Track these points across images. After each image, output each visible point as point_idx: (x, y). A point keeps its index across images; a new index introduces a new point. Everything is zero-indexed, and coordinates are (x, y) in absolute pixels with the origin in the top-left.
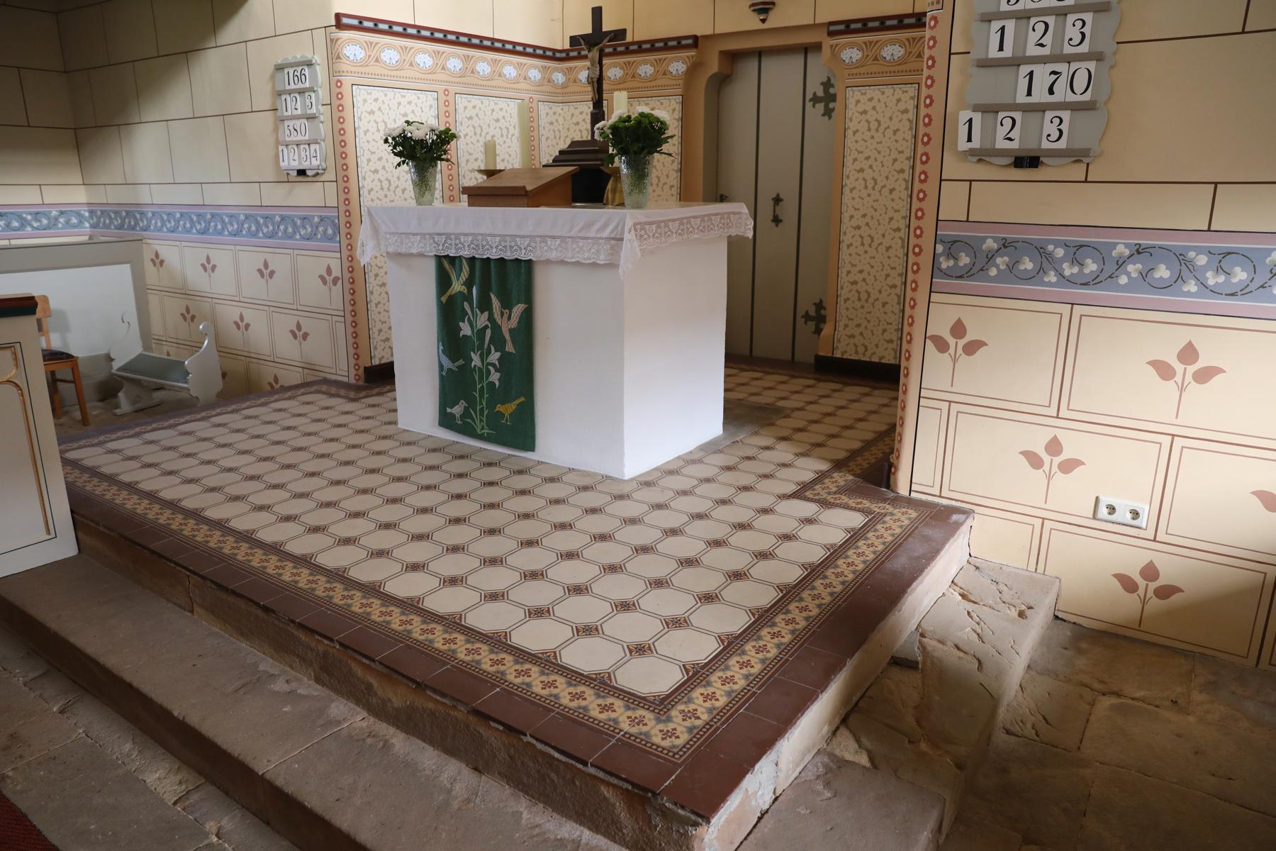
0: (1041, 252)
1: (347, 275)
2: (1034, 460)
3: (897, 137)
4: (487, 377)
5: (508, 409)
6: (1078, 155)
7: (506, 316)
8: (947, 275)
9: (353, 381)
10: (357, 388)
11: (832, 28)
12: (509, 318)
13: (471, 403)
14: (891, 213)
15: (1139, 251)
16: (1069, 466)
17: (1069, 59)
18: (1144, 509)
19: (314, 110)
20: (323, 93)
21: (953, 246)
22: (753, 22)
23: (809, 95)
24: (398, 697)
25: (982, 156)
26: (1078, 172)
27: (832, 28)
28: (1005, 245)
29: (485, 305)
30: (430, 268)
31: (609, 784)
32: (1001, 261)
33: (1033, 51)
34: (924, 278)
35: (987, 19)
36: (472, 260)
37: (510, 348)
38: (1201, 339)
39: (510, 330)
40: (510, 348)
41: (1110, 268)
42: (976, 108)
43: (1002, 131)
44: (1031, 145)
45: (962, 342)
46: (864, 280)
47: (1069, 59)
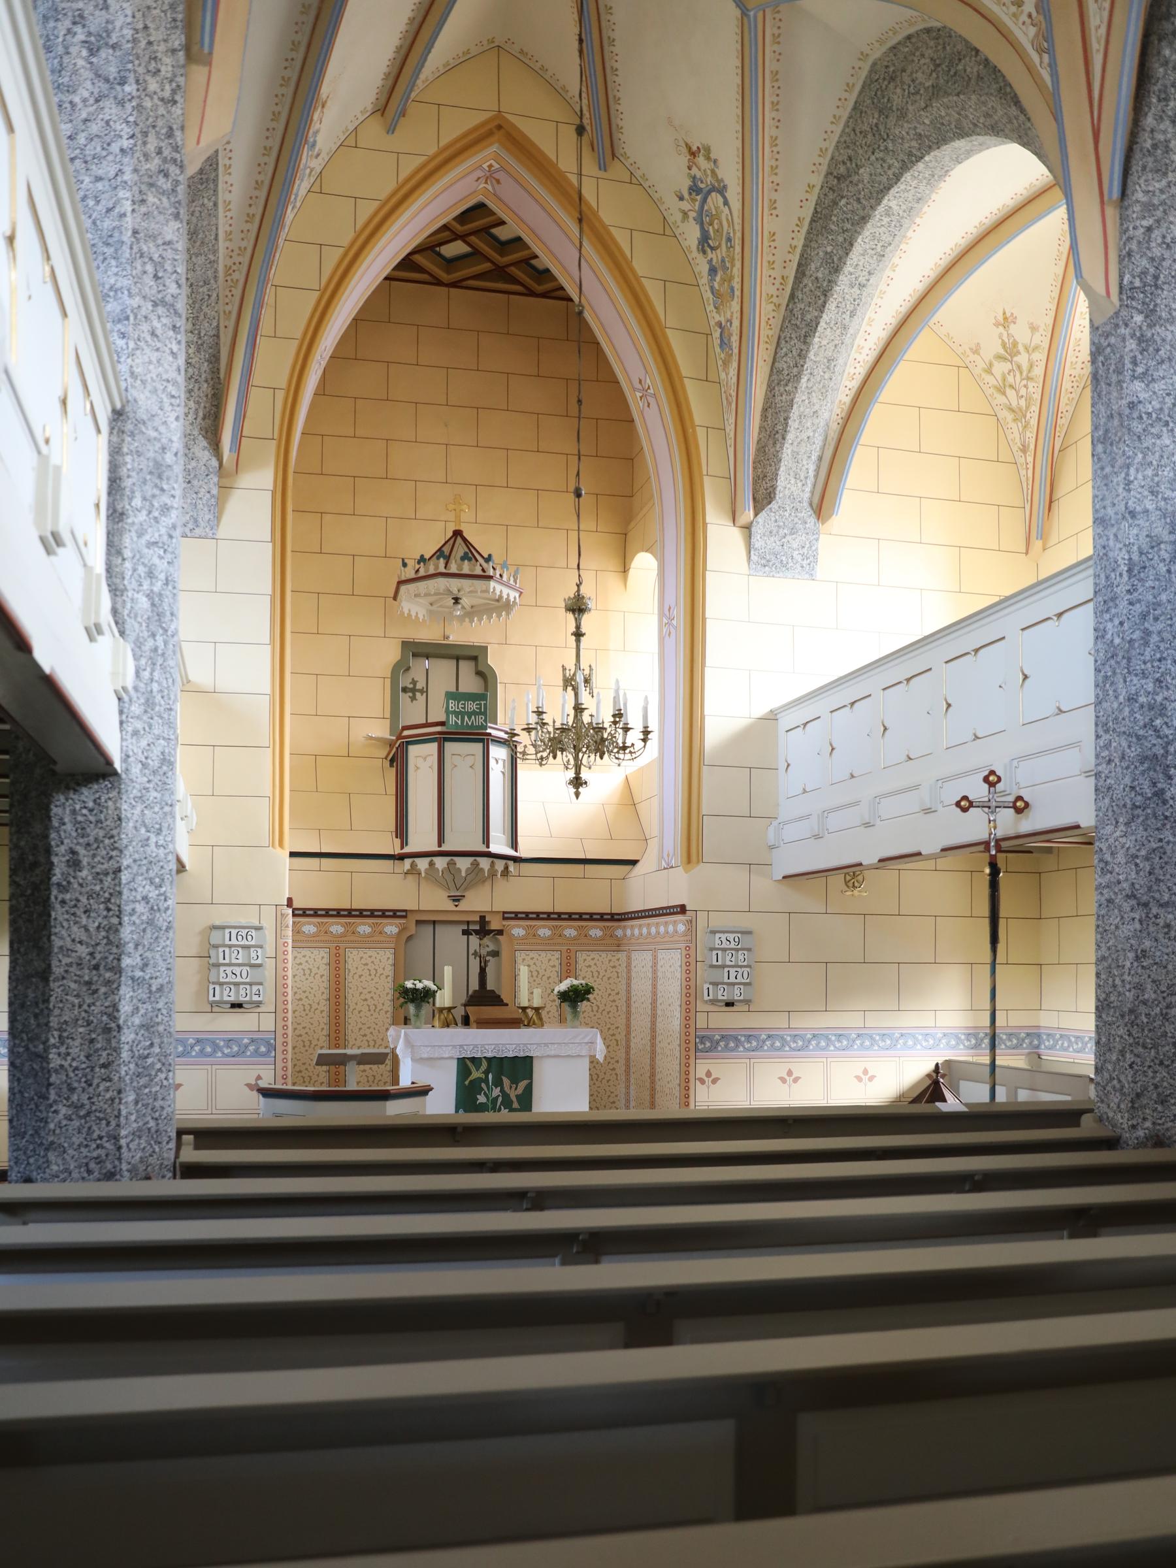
0: (736, 1039)
3: (550, 980)
6: (747, 1002)
11: (506, 915)
17: (741, 967)
19: (259, 961)
21: (703, 1039)
22: (450, 906)
23: (471, 951)
25: (714, 1002)
26: (746, 1008)
27: (506, 915)
28: (723, 1037)
29: (498, 1083)
30: (453, 1066)
32: (814, 1043)
33: (728, 963)
35: (712, 949)
36: (489, 1060)
38: (794, 1067)
39: (517, 1096)
41: (761, 1043)
42: (710, 983)
43: (720, 993)
45: (710, 1079)
47: (741, 967)
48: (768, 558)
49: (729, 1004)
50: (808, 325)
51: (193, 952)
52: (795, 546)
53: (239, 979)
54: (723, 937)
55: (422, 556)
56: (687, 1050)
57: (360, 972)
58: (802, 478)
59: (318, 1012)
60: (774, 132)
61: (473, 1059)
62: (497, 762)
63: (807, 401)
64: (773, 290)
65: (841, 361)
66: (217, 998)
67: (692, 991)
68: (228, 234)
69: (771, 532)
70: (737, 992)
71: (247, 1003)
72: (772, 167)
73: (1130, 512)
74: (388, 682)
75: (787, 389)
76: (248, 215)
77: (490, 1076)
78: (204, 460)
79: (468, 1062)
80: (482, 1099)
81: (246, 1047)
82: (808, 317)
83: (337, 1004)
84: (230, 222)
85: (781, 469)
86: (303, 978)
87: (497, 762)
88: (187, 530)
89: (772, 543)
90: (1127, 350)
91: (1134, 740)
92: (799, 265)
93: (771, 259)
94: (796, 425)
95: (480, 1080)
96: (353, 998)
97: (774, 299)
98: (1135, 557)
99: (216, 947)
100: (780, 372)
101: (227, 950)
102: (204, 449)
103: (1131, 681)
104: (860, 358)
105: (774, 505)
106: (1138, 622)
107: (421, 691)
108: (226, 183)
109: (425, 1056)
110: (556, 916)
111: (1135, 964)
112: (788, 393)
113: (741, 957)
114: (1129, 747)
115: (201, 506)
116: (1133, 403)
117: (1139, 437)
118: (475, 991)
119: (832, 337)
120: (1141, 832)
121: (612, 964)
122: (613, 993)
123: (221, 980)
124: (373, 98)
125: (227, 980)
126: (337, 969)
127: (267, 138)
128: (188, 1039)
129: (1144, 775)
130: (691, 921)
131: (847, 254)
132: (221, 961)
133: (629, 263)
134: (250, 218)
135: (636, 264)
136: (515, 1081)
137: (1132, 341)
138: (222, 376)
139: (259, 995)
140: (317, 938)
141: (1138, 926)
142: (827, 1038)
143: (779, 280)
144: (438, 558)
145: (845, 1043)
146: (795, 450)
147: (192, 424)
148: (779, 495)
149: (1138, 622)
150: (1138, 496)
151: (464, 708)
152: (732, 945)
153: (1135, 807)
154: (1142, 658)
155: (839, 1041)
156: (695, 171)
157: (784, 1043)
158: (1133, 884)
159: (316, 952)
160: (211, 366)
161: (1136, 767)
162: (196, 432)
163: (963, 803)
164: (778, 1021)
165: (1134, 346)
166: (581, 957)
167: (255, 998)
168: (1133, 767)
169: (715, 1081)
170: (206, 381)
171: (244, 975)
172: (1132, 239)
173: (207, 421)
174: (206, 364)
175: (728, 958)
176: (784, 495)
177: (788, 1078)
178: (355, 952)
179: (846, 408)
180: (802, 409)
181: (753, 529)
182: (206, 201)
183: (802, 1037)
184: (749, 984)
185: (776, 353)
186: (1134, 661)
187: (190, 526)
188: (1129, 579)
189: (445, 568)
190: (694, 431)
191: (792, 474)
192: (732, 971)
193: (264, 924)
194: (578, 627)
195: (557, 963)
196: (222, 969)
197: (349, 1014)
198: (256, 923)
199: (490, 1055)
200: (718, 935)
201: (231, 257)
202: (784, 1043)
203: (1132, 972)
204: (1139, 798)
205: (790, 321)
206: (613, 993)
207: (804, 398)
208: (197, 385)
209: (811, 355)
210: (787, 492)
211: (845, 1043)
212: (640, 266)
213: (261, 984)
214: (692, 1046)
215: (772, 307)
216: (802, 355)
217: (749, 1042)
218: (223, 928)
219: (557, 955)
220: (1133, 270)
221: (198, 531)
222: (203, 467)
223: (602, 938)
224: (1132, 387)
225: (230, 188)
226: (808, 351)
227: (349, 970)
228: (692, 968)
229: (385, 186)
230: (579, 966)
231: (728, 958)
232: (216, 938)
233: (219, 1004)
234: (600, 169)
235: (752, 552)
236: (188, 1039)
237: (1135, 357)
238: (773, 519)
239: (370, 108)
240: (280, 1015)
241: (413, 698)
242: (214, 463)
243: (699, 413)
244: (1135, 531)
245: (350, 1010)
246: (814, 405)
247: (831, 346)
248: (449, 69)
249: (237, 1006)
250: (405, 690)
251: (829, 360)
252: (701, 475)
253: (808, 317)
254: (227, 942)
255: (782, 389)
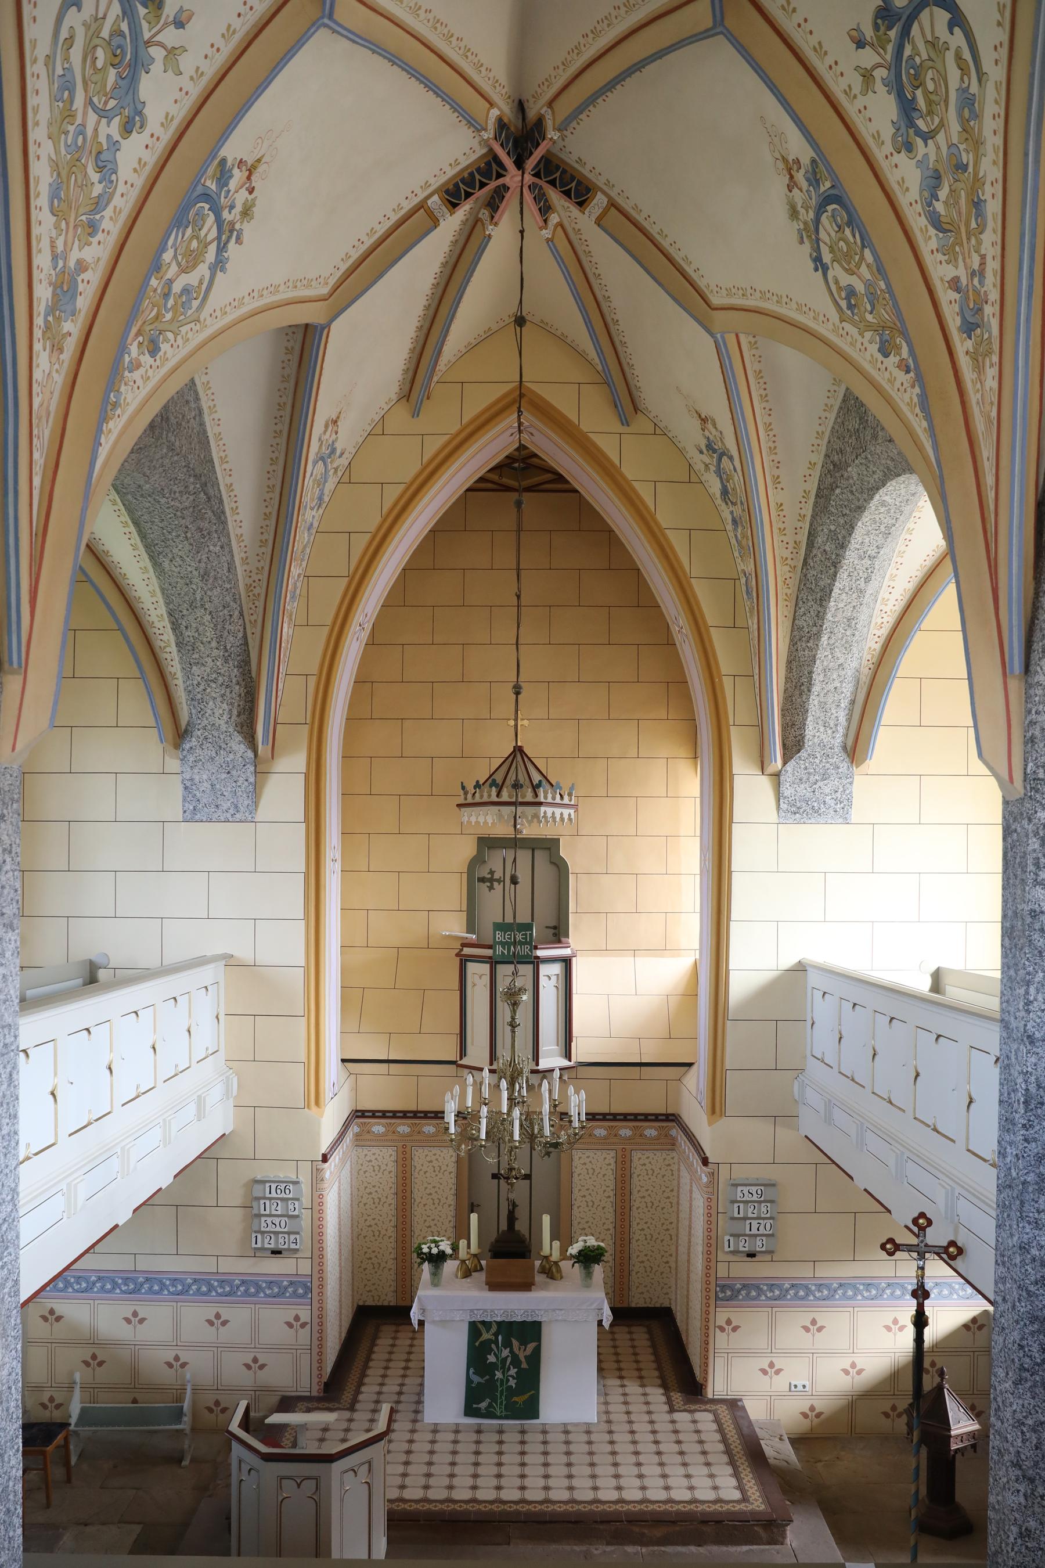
0: (758, 1288)
1: (316, 1320)
2: (764, 1372)
4: (507, 1383)
5: (519, 1399)
7: (522, 1350)
8: (722, 1299)
9: (315, 1393)
10: (319, 1399)
12: (525, 1350)
13: (494, 1399)
14: (604, 1220)
15: (793, 1286)
16: (778, 1372)
17: (764, 1219)
18: (807, 1383)
19: (296, 1213)
20: (306, 1201)
21: (723, 1288)
24: (658, 1532)
26: (768, 1257)
28: (744, 1286)
29: (507, 1344)
31: (757, 1525)
32: (743, 1292)
33: (750, 1215)
34: (712, 1302)
35: (733, 1202)
36: (499, 1323)
37: (524, 1365)
38: (818, 1317)
39: (526, 1357)
40: (524, 1365)
41: (784, 1293)
42: (731, 1236)
44: (753, 1249)
45: (730, 1327)
46: (436, 1192)
47: (764, 1219)
48: (798, 805)
49: (751, 1255)
50: (822, 590)
51: (238, 1202)
52: (827, 790)
53: (278, 1229)
54: (746, 1189)
55: (478, 782)
56: (708, 1298)
57: (425, 1169)
58: (832, 725)
59: (386, 1205)
60: (767, 419)
61: (483, 1323)
62: (550, 978)
63: (830, 656)
64: (787, 554)
65: (863, 618)
66: (259, 1245)
67: (713, 1242)
68: (245, 561)
69: (801, 780)
70: (759, 1243)
71: (285, 1249)
72: (770, 448)
73: (1029, 1037)
74: (465, 876)
75: (809, 645)
76: (261, 541)
77: (500, 1338)
78: (241, 753)
79: (480, 1326)
80: (491, 1359)
81: (286, 1288)
82: (821, 583)
83: (404, 1198)
84: (245, 550)
85: (809, 719)
86: (373, 1174)
87: (550, 978)
88: (229, 815)
89: (803, 790)
90: (1030, 848)
91: (1024, 1294)
92: (809, 533)
93: (782, 526)
94: (821, 677)
95: (490, 1341)
96: (419, 1191)
97: (789, 561)
98: (1033, 1088)
99: (258, 1199)
100: (800, 629)
101: (268, 1203)
102: (240, 743)
103: (1024, 1227)
104: (887, 609)
105: (803, 754)
106: (1033, 1163)
107: (499, 881)
108: (236, 521)
109: (437, 1319)
110: (611, 1117)
111: (1019, 1541)
112: (811, 649)
113: (764, 1209)
114: (1019, 1300)
115: (240, 793)
116: (1035, 911)
117: (1040, 952)
118: (503, 1231)
119: (849, 600)
120: (1028, 1399)
121: (667, 1162)
122: (668, 1190)
123: (263, 1229)
124: (396, 389)
125: (268, 1229)
126: (404, 1166)
127: (269, 479)
128: (234, 1280)
129: (1033, 1337)
130: (713, 1173)
131: (850, 535)
132: (262, 1212)
133: (653, 517)
134: (263, 543)
135: (659, 517)
136: (524, 1343)
137: (1034, 840)
138: (254, 675)
139: (296, 1243)
140: (386, 1138)
141: (1022, 1500)
142: (854, 1287)
143: (791, 545)
144: (491, 786)
145: (874, 1292)
146: (822, 700)
147: (227, 723)
148: (808, 744)
149: (1033, 1163)
150: (1038, 1021)
151: (510, 939)
152: (755, 1198)
153: (1022, 1368)
154: (1036, 1205)
155: (867, 1290)
156: (707, 433)
157: (808, 1291)
158: (1018, 1452)
159: (384, 1150)
160: (241, 670)
161: (1025, 1325)
162: (231, 730)
163: (888, 1246)
164: (803, 1271)
165: (1036, 846)
166: (636, 1155)
167: (293, 1246)
168: (1022, 1323)
169: (735, 1329)
170: (238, 683)
171: (283, 1224)
172: (1035, 723)
173: (242, 716)
174: (235, 670)
175: (750, 1210)
176: (814, 743)
177: (811, 1327)
178: (420, 1150)
179: (877, 653)
180: (825, 663)
181: (782, 778)
182: (211, 548)
183: (828, 1287)
184: (772, 1235)
185: (795, 612)
186: (1027, 1207)
187: (232, 811)
188: (1026, 1112)
189: (498, 796)
190: (721, 680)
191: (820, 722)
192: (754, 1223)
193: (301, 1179)
194: (513, 1018)
195: (612, 1161)
196: (263, 1219)
197: (415, 1207)
198: (294, 1178)
199: (499, 1319)
200: (740, 1189)
201: (250, 577)
202: (808, 1291)
203: (1016, 1549)
204: (1028, 1360)
205: (805, 585)
206: (668, 1190)
207: (826, 654)
208: (228, 690)
209: (829, 616)
210: (816, 740)
211: (874, 1292)
212: (664, 518)
213: (298, 1233)
214: (712, 1295)
215: (787, 568)
216: (820, 616)
217: (772, 1291)
218: (264, 1182)
219: (613, 1153)
220: (1036, 759)
221: (238, 816)
222: (240, 759)
223: (657, 1138)
224: (1033, 892)
225: (240, 524)
226: (825, 613)
227: (415, 1167)
228: (714, 1219)
229: (411, 469)
230: (634, 1165)
231: (750, 1210)
232: (258, 1191)
233: (263, 1249)
234: (623, 424)
235: (781, 801)
236: (234, 1280)
237: (1038, 858)
238: (803, 766)
239: (395, 398)
240: (316, 1260)
241: (491, 888)
242: (250, 754)
243: (725, 664)
244: (1033, 1060)
245: (416, 1203)
246: (838, 659)
247: (850, 608)
248: (471, 348)
249: (276, 1252)
250: (482, 880)
251: (848, 620)
252: (728, 726)
253: (821, 583)
254: (268, 1195)
255: (804, 645)
